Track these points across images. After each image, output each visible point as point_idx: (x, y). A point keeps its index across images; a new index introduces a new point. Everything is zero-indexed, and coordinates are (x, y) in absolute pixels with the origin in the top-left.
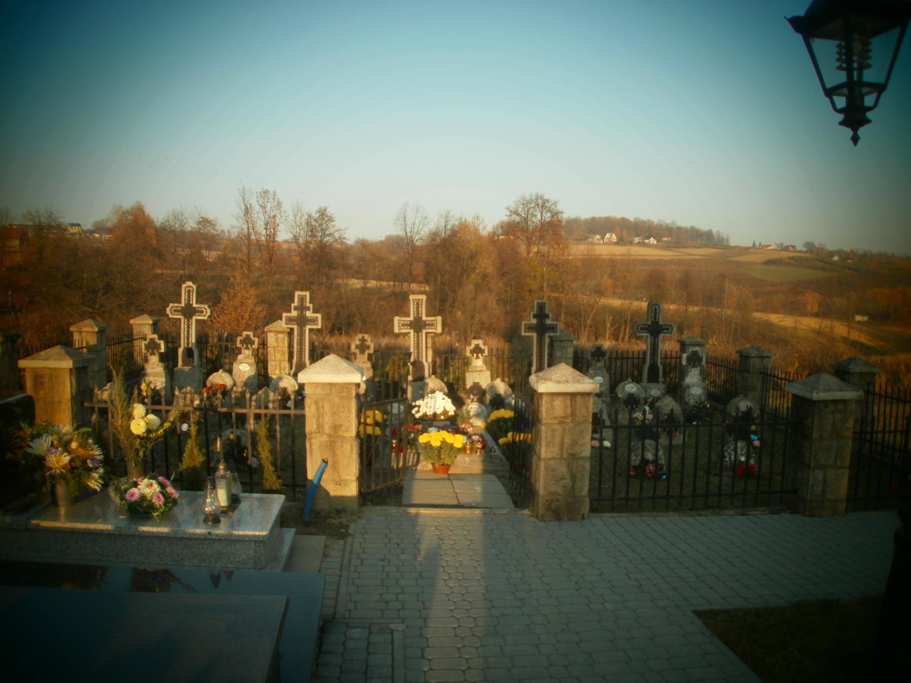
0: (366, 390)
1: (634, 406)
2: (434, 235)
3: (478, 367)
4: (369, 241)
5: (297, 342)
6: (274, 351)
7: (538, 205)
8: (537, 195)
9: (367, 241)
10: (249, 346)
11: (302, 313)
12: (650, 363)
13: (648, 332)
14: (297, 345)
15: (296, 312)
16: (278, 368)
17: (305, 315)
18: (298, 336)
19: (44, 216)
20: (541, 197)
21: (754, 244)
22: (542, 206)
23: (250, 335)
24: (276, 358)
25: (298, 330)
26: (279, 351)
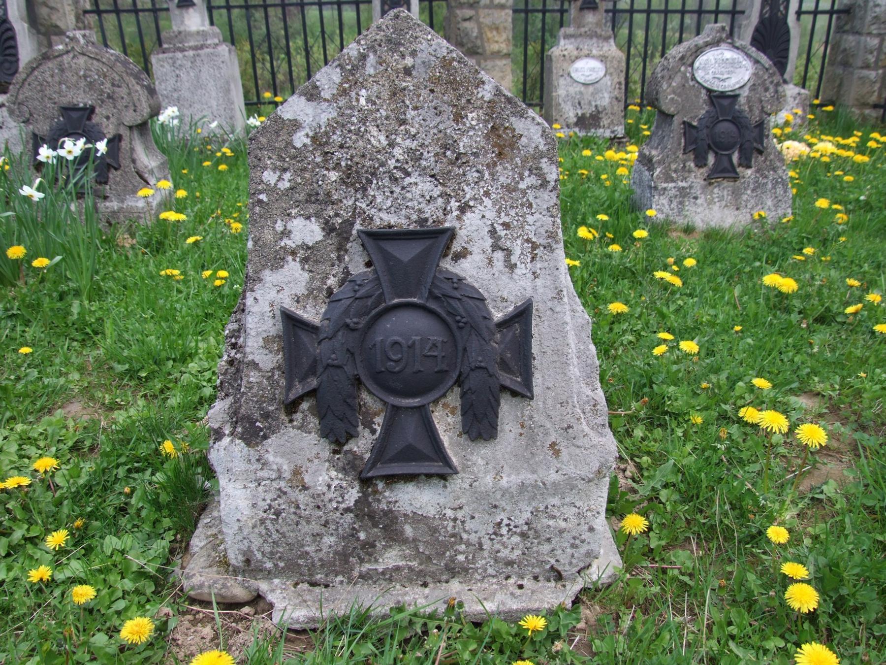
1: (735, 158)
3: (189, 34)
12: (761, 14)
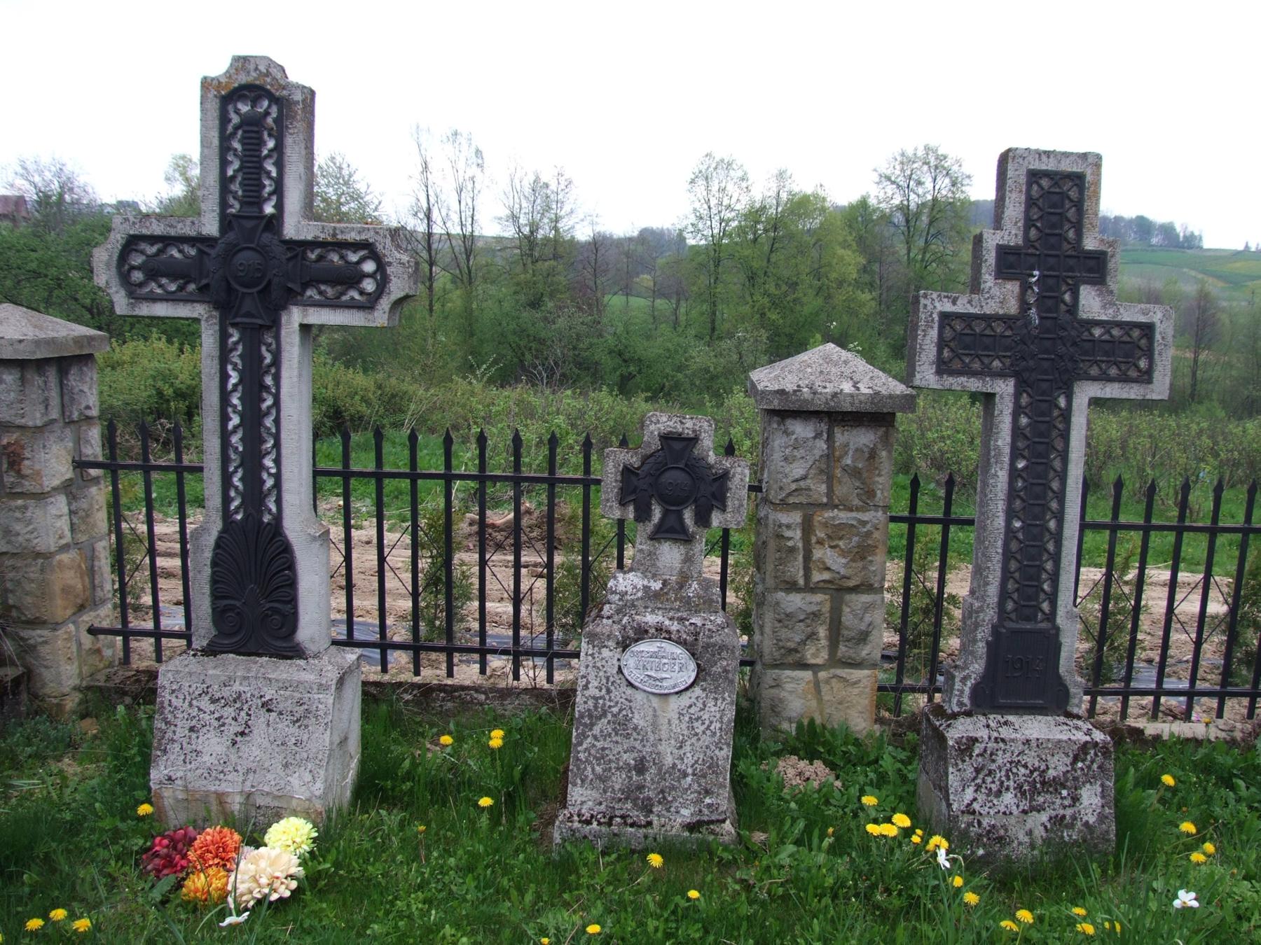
0: (260, 350)
2: (755, 215)
4: (615, 237)
5: (1012, 494)
6: (807, 527)
7: (928, 163)
8: (927, 149)
9: (611, 236)
10: (688, 516)
11: (1049, 300)
13: (203, 294)
14: (1010, 514)
15: (1012, 288)
16: (822, 632)
17: (1074, 307)
18: (1015, 454)
19: (50, 171)
20: (935, 151)
21: (1247, 246)
22: (936, 167)
23: (694, 440)
24: (817, 577)
25: (1017, 411)
26: (836, 533)
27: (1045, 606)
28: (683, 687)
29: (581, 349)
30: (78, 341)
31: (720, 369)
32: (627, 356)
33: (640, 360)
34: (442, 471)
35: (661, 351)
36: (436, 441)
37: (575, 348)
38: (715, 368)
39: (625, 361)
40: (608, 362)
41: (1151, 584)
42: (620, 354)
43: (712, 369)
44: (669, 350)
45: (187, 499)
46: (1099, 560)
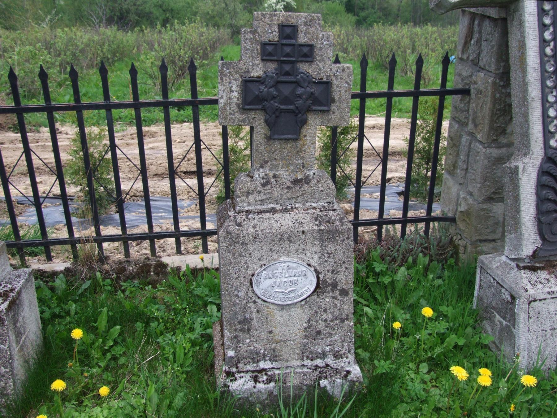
27: (549, 83)
28: (309, 294)
29: (139, 5)
30: (417, 53)
31: (215, 13)
32: (164, 8)
33: (172, 10)
34: (159, 98)
35: (184, 4)
36: (95, 76)
37: (135, 5)
38: (212, 12)
39: (164, 11)
40: (157, 12)
41: (363, 201)
42: (161, 6)
43: (210, 13)
44: (189, 4)
45: (29, 141)
46: (191, 214)
